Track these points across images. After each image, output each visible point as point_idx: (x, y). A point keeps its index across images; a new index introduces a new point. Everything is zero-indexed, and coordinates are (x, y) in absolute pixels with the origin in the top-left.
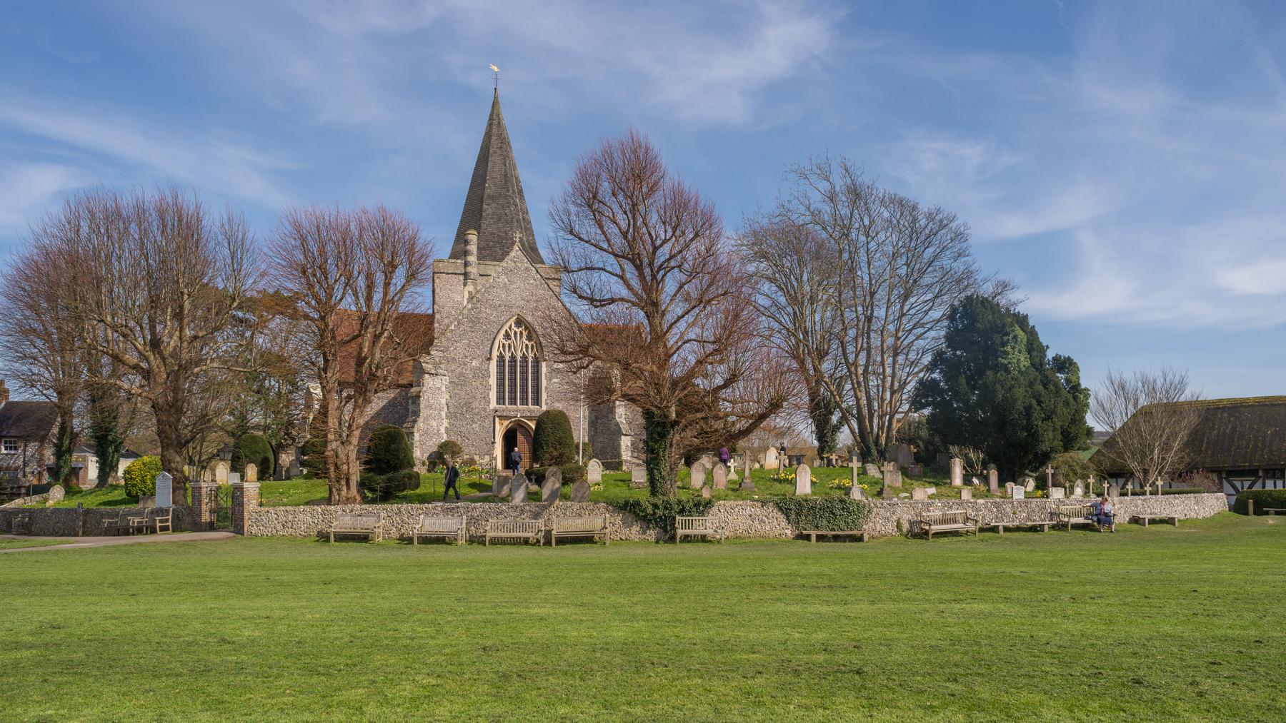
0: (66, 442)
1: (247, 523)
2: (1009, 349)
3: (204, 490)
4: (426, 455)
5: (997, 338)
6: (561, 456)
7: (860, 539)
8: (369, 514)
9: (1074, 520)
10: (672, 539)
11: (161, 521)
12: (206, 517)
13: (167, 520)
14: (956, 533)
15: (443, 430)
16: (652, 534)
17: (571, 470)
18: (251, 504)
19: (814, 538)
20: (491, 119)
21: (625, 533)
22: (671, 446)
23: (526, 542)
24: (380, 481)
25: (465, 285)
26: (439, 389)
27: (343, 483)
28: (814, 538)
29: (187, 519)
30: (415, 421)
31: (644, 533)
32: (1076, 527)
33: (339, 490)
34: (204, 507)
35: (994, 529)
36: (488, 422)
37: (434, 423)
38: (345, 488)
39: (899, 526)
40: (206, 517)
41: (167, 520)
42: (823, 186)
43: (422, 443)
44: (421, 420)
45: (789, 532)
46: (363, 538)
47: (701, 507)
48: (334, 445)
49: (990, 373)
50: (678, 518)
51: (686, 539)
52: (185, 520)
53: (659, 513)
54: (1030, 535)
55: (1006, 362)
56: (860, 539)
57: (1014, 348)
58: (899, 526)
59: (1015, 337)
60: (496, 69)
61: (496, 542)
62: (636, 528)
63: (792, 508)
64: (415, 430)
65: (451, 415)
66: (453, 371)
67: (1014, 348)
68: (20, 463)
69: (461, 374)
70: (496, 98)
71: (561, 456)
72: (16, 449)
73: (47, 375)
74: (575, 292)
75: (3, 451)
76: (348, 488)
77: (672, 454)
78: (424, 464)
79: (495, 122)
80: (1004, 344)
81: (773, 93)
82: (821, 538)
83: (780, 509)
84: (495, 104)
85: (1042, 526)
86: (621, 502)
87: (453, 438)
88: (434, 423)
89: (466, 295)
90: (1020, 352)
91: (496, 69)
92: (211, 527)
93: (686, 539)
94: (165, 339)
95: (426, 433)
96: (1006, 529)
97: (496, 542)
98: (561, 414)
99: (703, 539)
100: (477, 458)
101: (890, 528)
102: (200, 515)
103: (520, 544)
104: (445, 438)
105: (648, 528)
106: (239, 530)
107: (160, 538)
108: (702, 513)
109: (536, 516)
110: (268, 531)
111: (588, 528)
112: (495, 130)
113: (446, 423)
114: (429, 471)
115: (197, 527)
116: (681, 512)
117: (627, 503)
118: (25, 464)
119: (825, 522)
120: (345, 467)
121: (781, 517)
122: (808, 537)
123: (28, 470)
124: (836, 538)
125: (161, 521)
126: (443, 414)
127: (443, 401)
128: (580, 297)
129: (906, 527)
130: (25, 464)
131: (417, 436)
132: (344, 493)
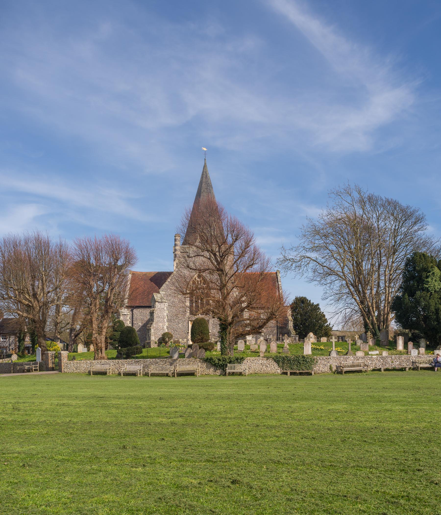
0: (22, 335)
1: (63, 368)
2: (429, 280)
3: (49, 355)
4: (157, 339)
5: (424, 274)
6: (202, 338)
7: (311, 374)
8: (107, 364)
9: (421, 366)
10: (225, 375)
11: (34, 367)
12: (50, 365)
13: (37, 367)
14: (360, 371)
15: (165, 327)
16: (219, 372)
17: (206, 345)
18: (65, 360)
19: (289, 373)
20: (203, 175)
21: (207, 371)
22: (230, 333)
23: (167, 375)
24: (125, 350)
25: (174, 260)
26: (163, 309)
27: (99, 351)
28: (289, 373)
29: (45, 366)
30: (152, 324)
31: (215, 371)
32: (422, 368)
33: (98, 354)
34: (50, 361)
35: (380, 370)
36: (185, 324)
37: (161, 324)
38: (100, 353)
39: (331, 368)
40: (50, 365)
41: (37, 367)
42: (349, 199)
43: (155, 334)
44: (154, 323)
45: (279, 371)
46: (104, 373)
47: (240, 360)
48: (95, 335)
49: (418, 293)
50: (228, 365)
51: (233, 374)
52: (44, 367)
53: (221, 363)
54: (400, 373)
55: (427, 286)
56: (311, 374)
57: (432, 279)
58: (331, 368)
59: (433, 273)
60: (205, 149)
61: (153, 375)
62: (212, 370)
63: (279, 360)
64: (152, 328)
65: (169, 321)
66: (170, 300)
67: (432, 279)
68: (8, 345)
69: (173, 301)
70: (205, 164)
71: (202, 338)
72: (6, 339)
73: (14, 307)
74: (188, 267)
75: (1, 340)
76: (102, 353)
77: (230, 338)
78: (156, 343)
79: (205, 176)
80: (427, 277)
81: (383, 132)
82: (292, 374)
83: (275, 361)
84: (205, 166)
85: (405, 368)
86: (206, 358)
87: (170, 331)
88: (161, 324)
89: (175, 265)
90: (436, 281)
91: (205, 149)
92: (53, 369)
93: (233, 374)
94: (38, 293)
95: (157, 329)
96: (387, 370)
97: (153, 375)
98: (203, 319)
99: (240, 374)
100: (180, 340)
101: (326, 369)
102: (48, 365)
103: (164, 376)
104: (166, 331)
105: (217, 369)
106: (60, 370)
107: (35, 373)
108: (240, 363)
109: (171, 364)
110: (71, 371)
111: (192, 369)
112: (204, 180)
113: (167, 324)
114: (158, 346)
115: (48, 369)
116: (230, 362)
117: (208, 358)
118: (10, 345)
119: (295, 367)
120: (100, 344)
121: (276, 365)
122: (286, 373)
123: (11, 347)
124: (301, 374)
125: (34, 367)
126: (165, 320)
127: (165, 314)
128: (191, 269)
129: (334, 369)
130: (10, 345)
131: (152, 331)
132: (100, 355)
